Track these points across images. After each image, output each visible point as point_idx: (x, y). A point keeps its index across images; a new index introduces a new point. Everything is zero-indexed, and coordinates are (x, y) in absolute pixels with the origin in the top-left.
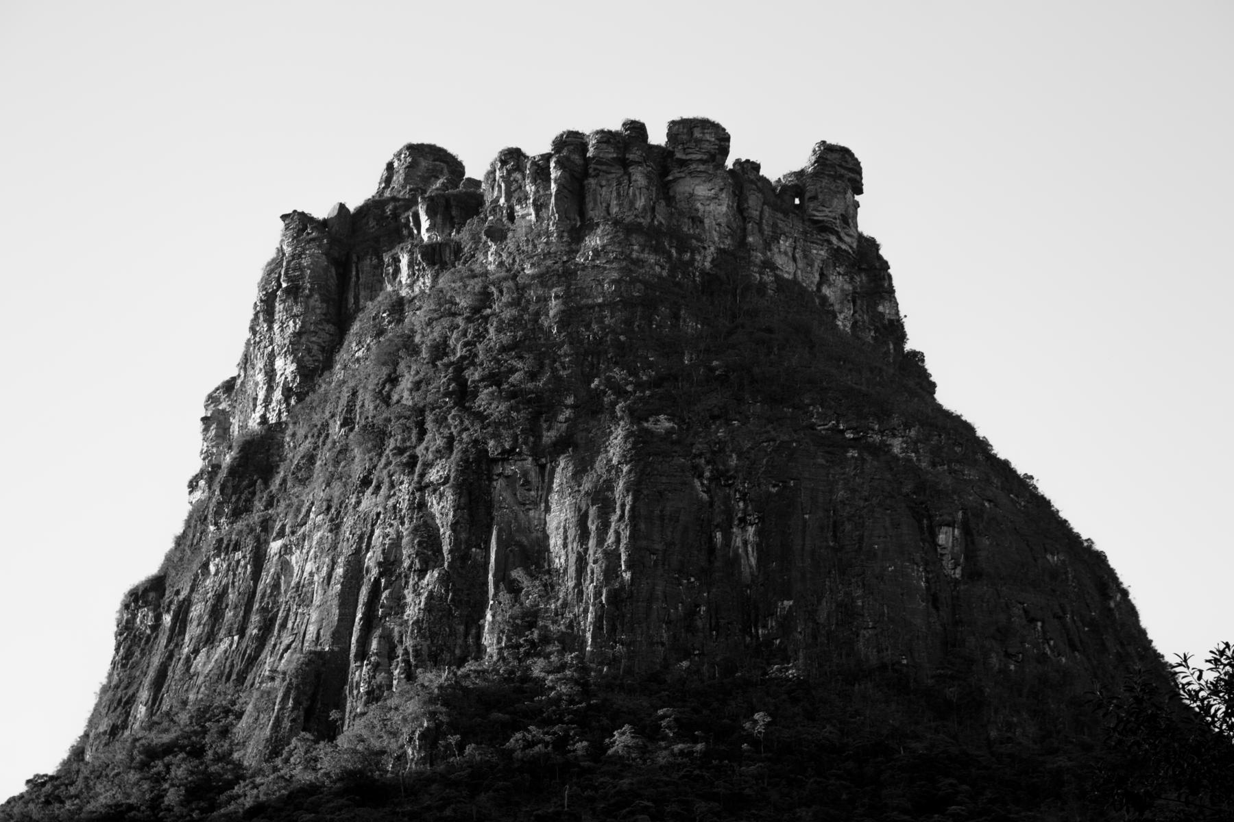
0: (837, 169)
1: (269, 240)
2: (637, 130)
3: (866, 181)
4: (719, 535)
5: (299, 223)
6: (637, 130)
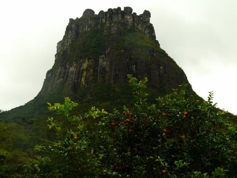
0: (147, 14)
1: (67, 23)
2: (119, 8)
3: (151, 16)
4: (41, 174)
5: (71, 20)
6: (119, 8)
